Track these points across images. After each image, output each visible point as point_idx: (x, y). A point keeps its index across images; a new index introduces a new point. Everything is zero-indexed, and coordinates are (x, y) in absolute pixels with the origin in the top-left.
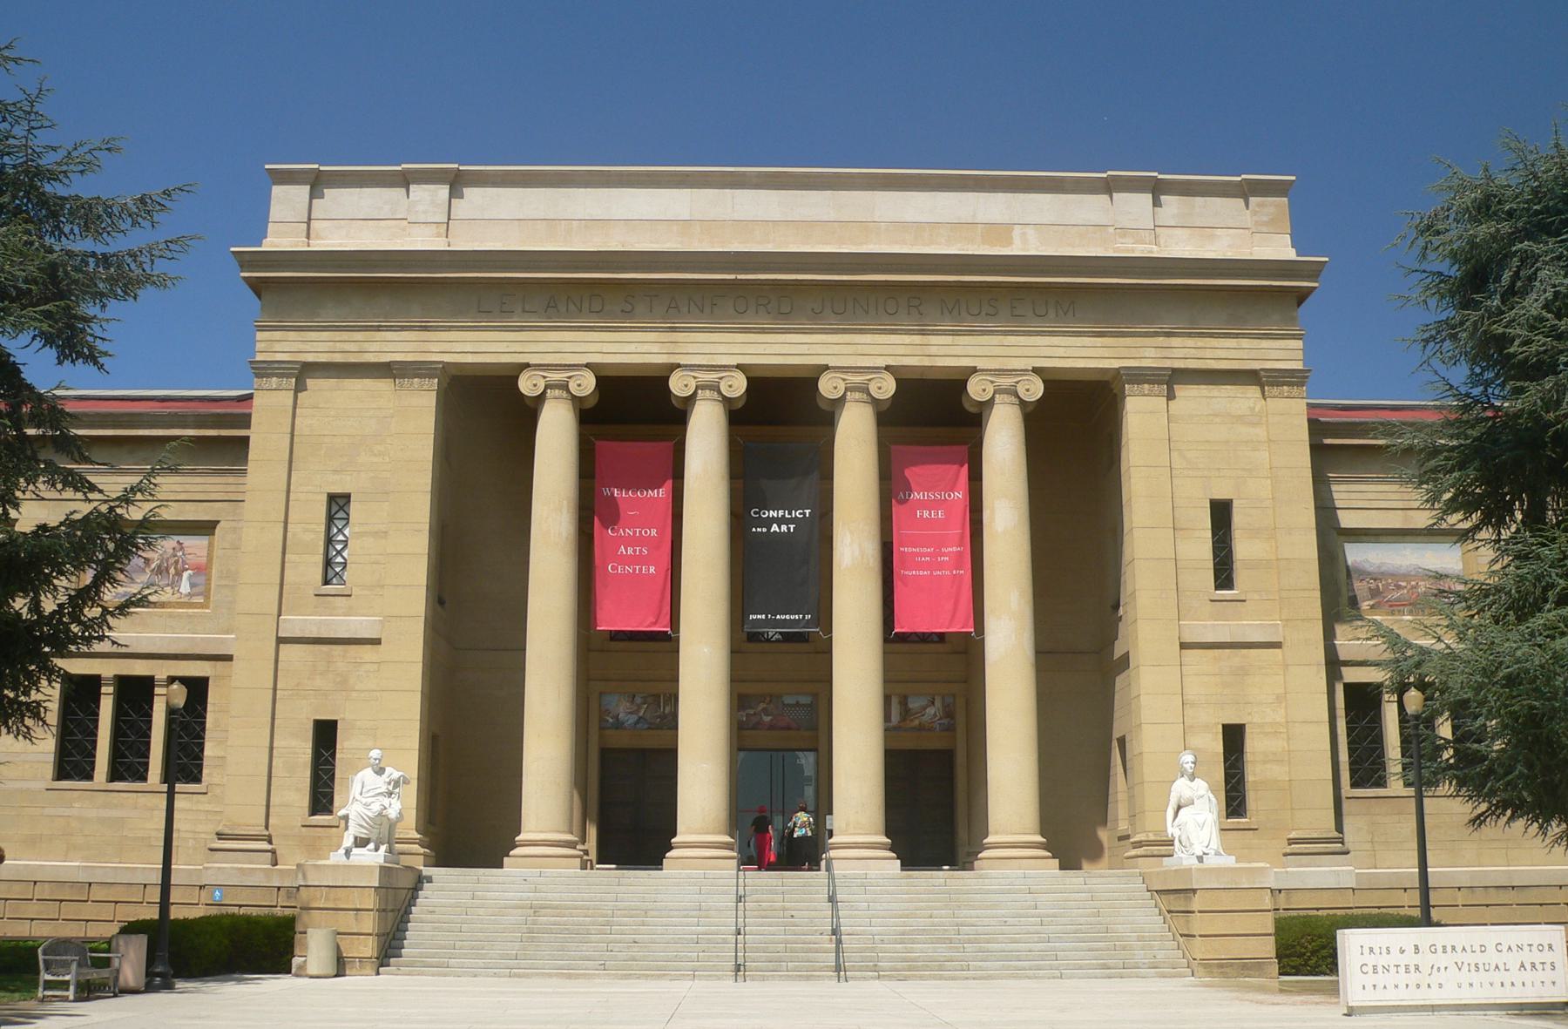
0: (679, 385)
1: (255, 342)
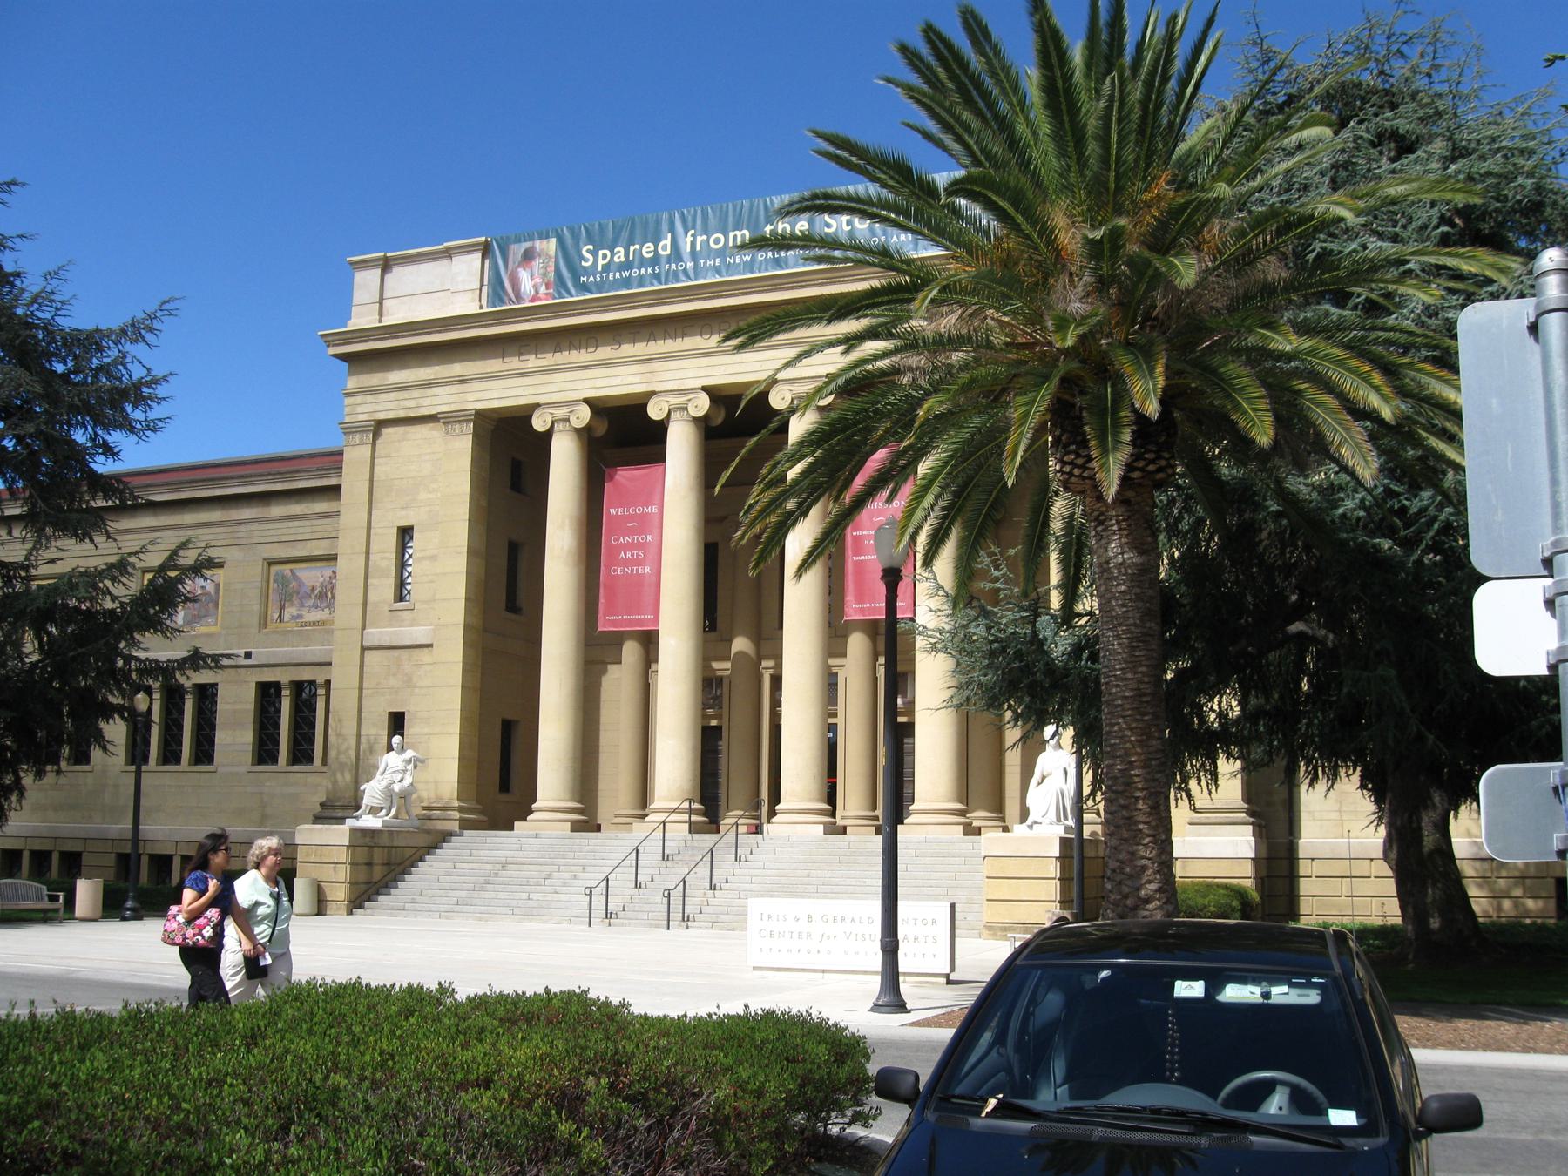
0: (655, 412)
1: (343, 406)
